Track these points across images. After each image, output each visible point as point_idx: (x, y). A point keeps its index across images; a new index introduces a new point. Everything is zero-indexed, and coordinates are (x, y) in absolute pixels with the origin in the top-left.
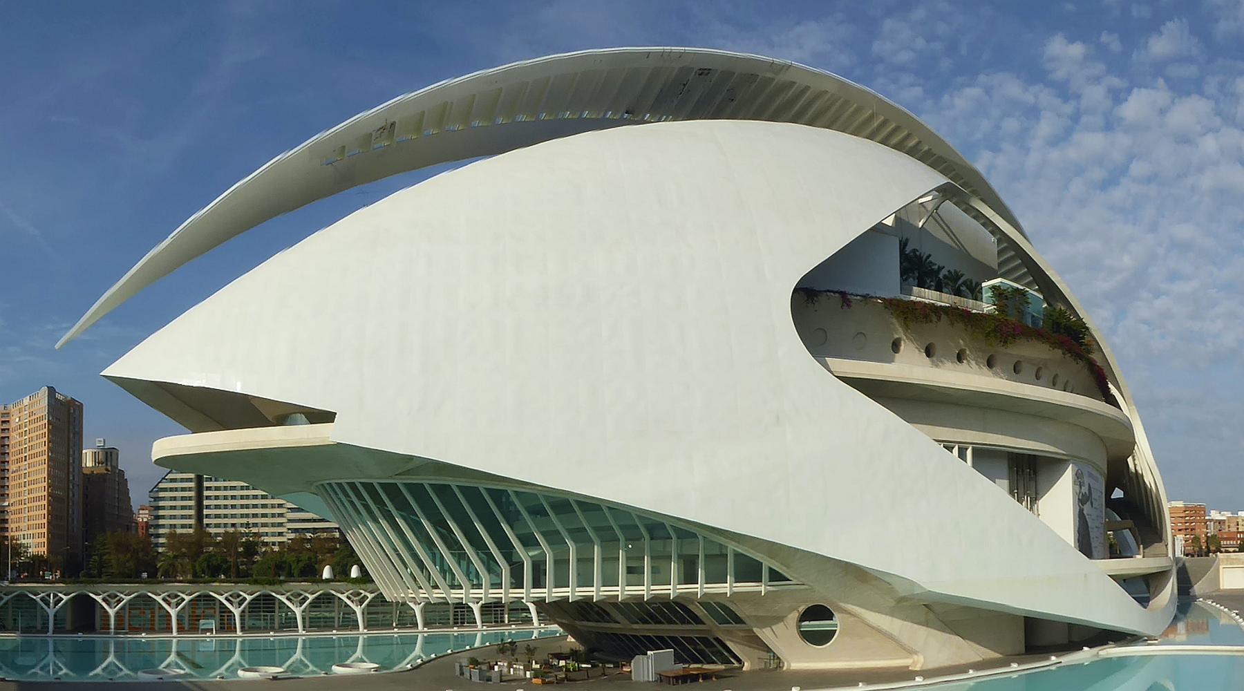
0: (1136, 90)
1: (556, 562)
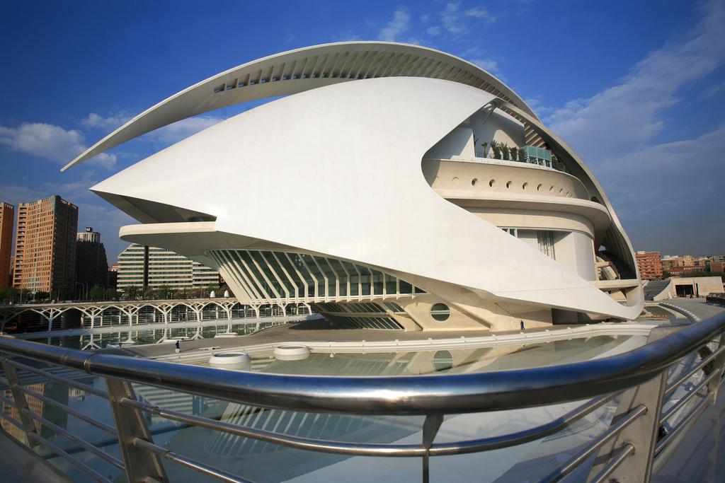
0: (720, 278)
1: (319, 286)
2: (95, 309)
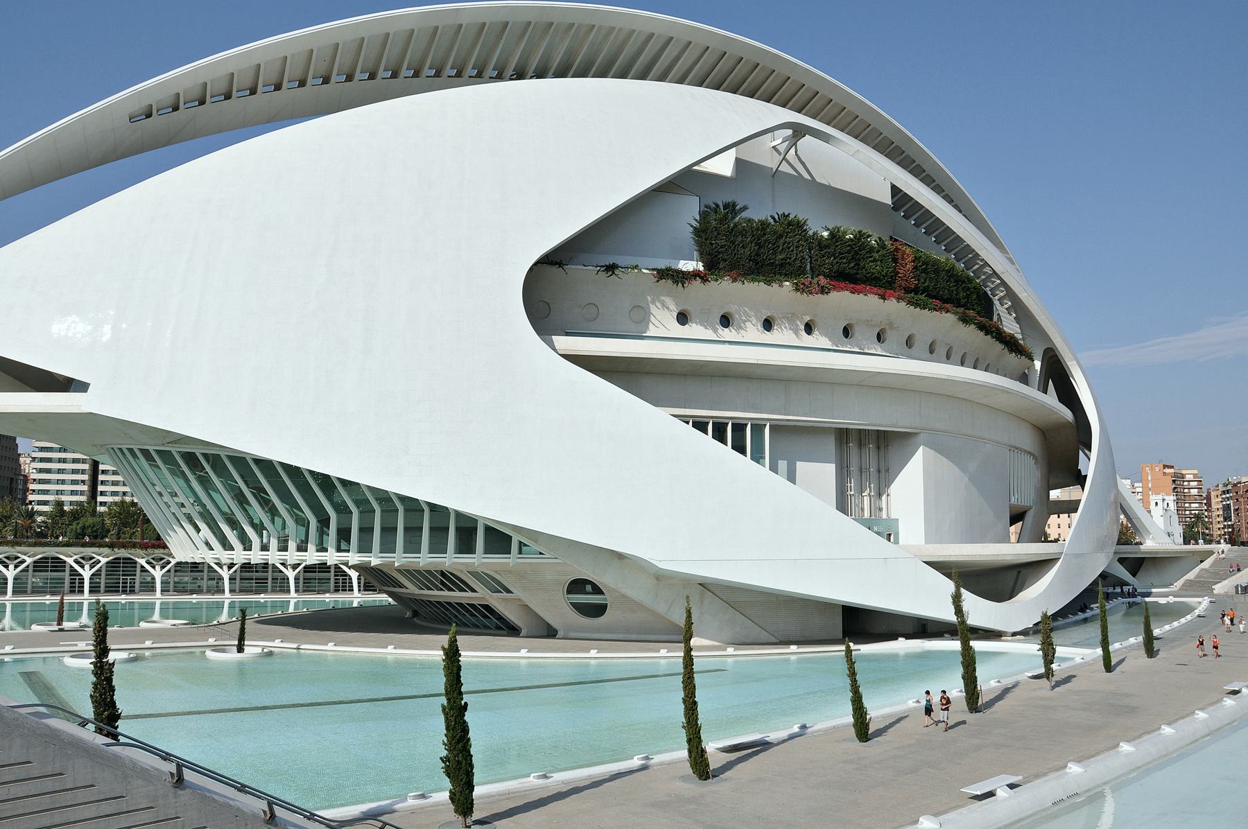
1: (361, 530)
2: (92, 558)
